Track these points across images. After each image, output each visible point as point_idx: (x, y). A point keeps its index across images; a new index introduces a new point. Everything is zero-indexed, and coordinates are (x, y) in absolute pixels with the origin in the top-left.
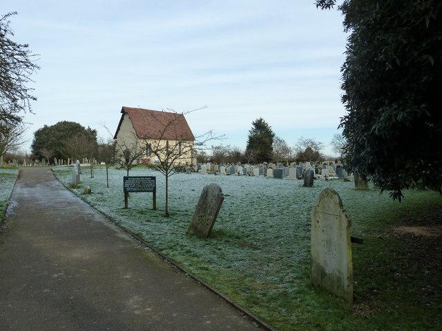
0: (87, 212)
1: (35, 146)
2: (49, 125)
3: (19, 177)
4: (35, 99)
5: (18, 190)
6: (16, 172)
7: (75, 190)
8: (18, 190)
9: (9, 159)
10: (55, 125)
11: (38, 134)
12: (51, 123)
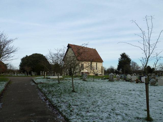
1: (22, 65)
2: (28, 55)
10: (31, 55)
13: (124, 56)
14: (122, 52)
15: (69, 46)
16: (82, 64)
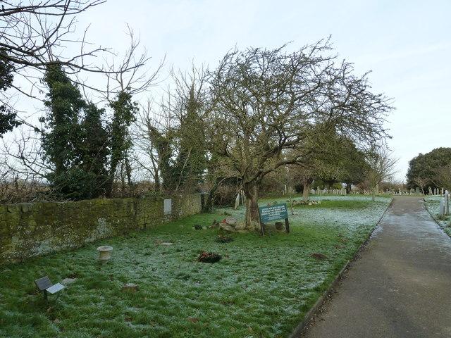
0: (445, 245)
1: (411, 175)
2: (424, 153)
3: (391, 205)
4: (391, 138)
5: (387, 217)
6: (389, 200)
7: (441, 222)
8: (387, 217)
9: (386, 188)
10: (430, 153)
11: (413, 163)
12: (426, 150)
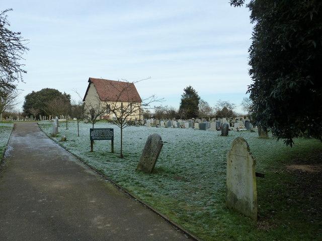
0: (64, 154)
1: (26, 106)
2: (36, 91)
3: (14, 129)
4: (25, 72)
5: (13, 138)
6: (12, 125)
7: (55, 139)
8: (13, 138)
9: (6, 116)
10: (40, 91)
11: (28, 97)
12: (37, 89)
13: (189, 91)
14: (186, 87)
15: (91, 81)
16: (311, 42)
